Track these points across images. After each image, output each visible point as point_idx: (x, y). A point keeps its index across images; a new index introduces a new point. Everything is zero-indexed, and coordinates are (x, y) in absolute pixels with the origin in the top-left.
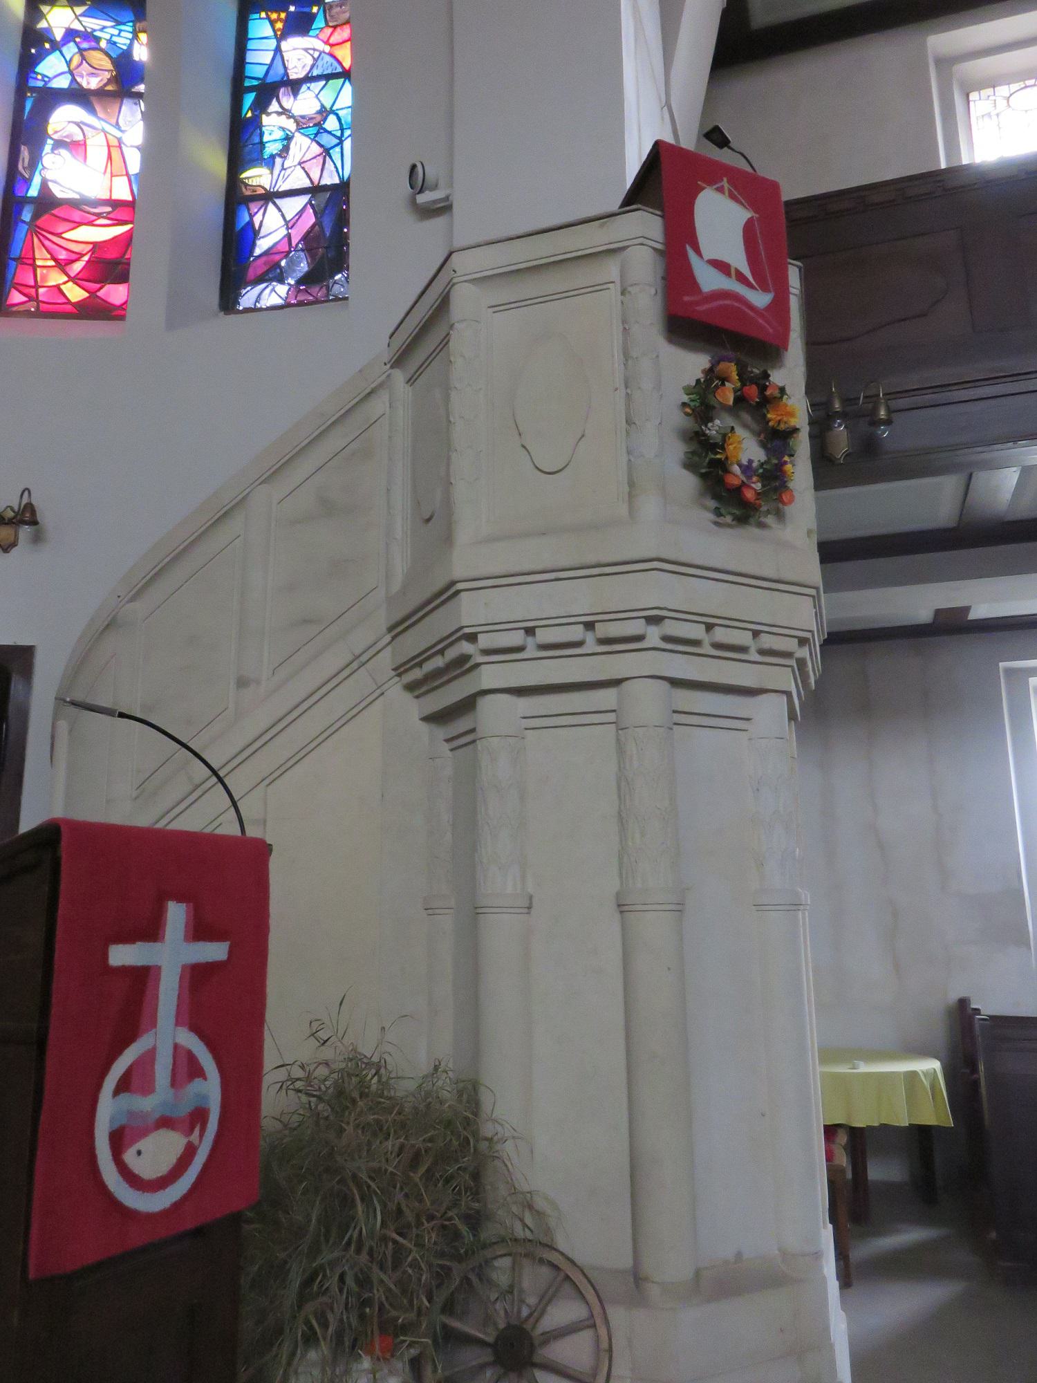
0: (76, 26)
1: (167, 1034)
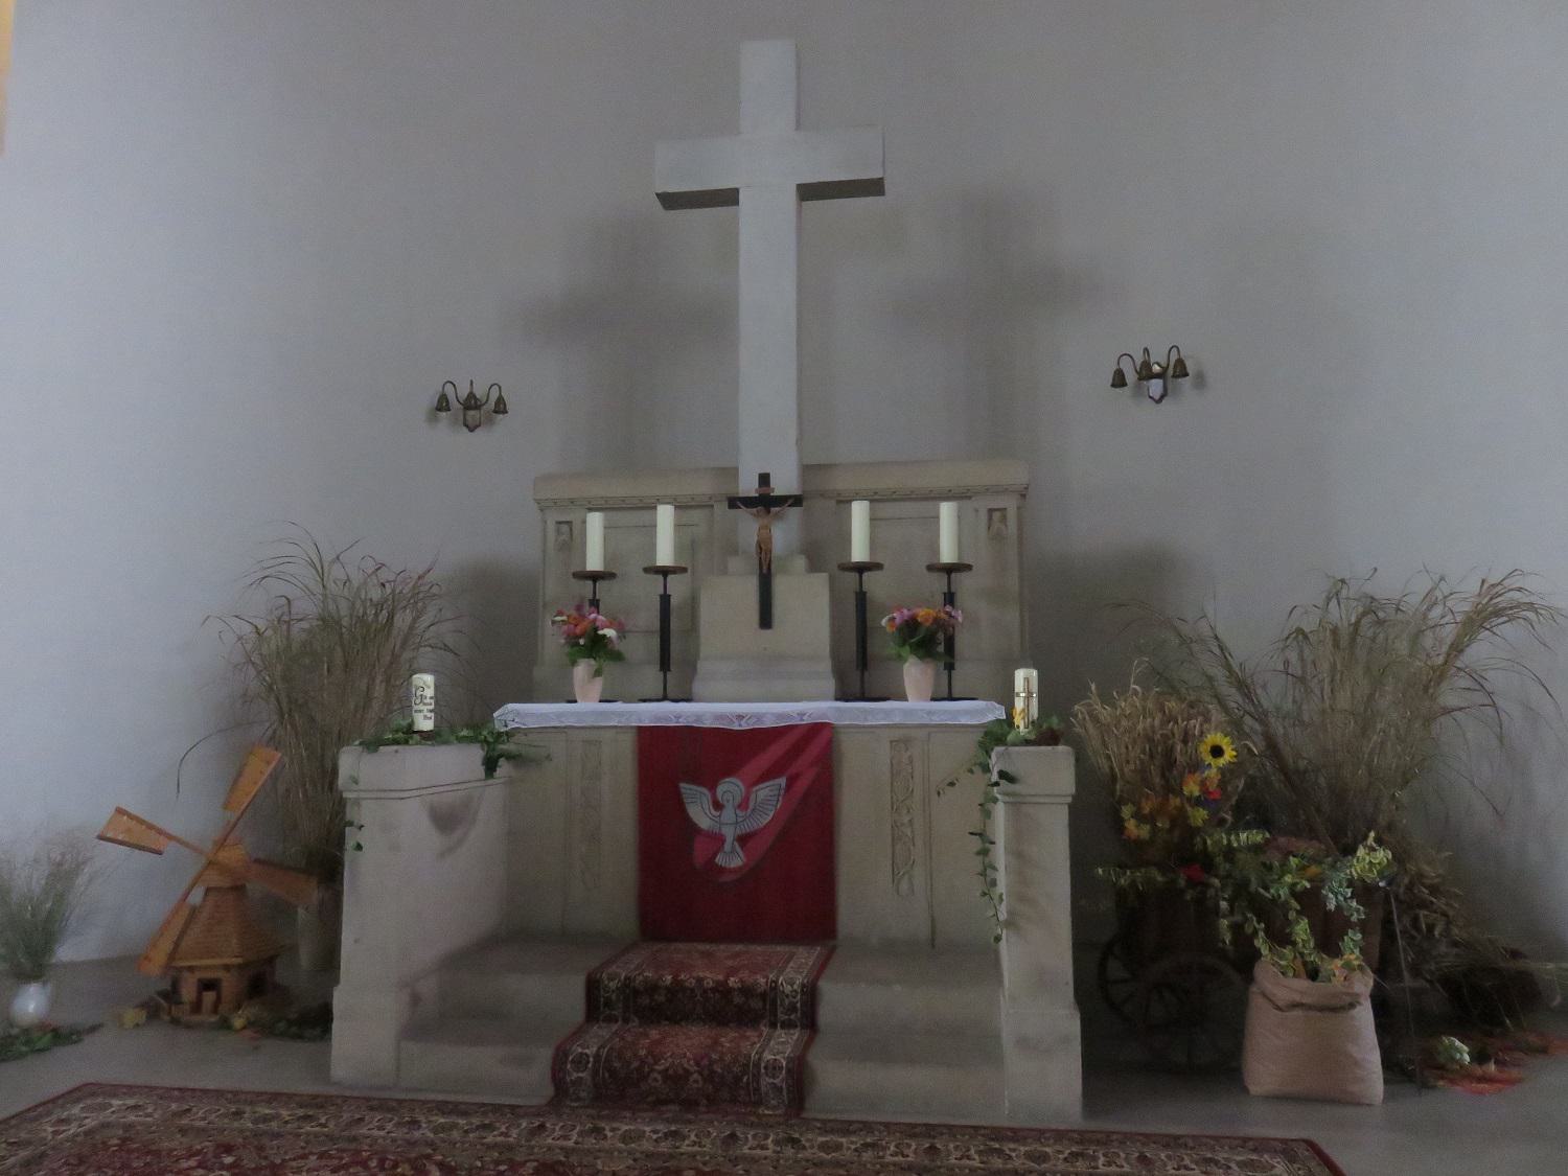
0: (800, 563)
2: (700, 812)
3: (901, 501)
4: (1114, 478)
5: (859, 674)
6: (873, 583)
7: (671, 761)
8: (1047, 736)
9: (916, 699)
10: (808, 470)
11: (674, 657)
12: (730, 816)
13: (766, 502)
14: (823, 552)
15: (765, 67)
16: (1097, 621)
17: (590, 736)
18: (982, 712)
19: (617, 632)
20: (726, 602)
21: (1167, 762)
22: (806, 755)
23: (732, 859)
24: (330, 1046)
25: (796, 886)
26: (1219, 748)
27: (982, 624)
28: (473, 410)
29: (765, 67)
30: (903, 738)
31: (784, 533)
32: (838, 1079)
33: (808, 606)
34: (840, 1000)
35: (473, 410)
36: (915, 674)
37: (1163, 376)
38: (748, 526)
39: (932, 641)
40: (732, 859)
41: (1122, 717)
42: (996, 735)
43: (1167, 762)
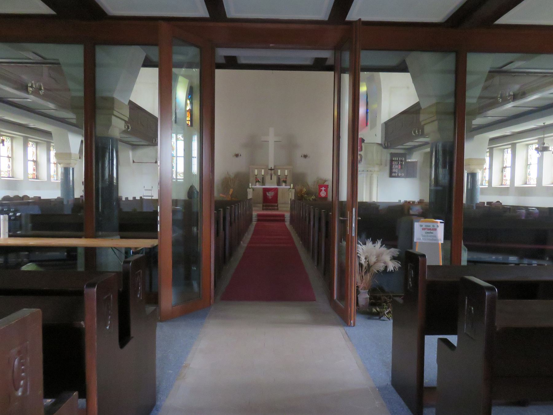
1: (323, 191)
2: (268, 194)
3: (283, 169)
4: (301, 165)
5: (279, 184)
6: (280, 177)
7: (266, 190)
8: (293, 188)
9: (283, 186)
10: (275, 166)
11: (263, 183)
12: (270, 195)
13: (271, 169)
14: (276, 173)
15: (271, 131)
16: (298, 179)
17: (259, 188)
18: (288, 187)
19: (430, 203)
20: (268, 178)
21: (301, 191)
22: (276, 190)
23: (270, 198)
24: (44, 320)
25: (275, 197)
26: (305, 190)
27: (289, 180)
28: (237, 155)
29: (271, 131)
30: (283, 189)
31: (273, 172)
32: (280, 209)
33: (275, 178)
34: (279, 206)
35: (237, 155)
36: (284, 184)
37: (305, 156)
38: (270, 172)
39: (285, 182)
40: (270, 198)
41: (299, 188)
42: (290, 188)
43: (301, 191)
